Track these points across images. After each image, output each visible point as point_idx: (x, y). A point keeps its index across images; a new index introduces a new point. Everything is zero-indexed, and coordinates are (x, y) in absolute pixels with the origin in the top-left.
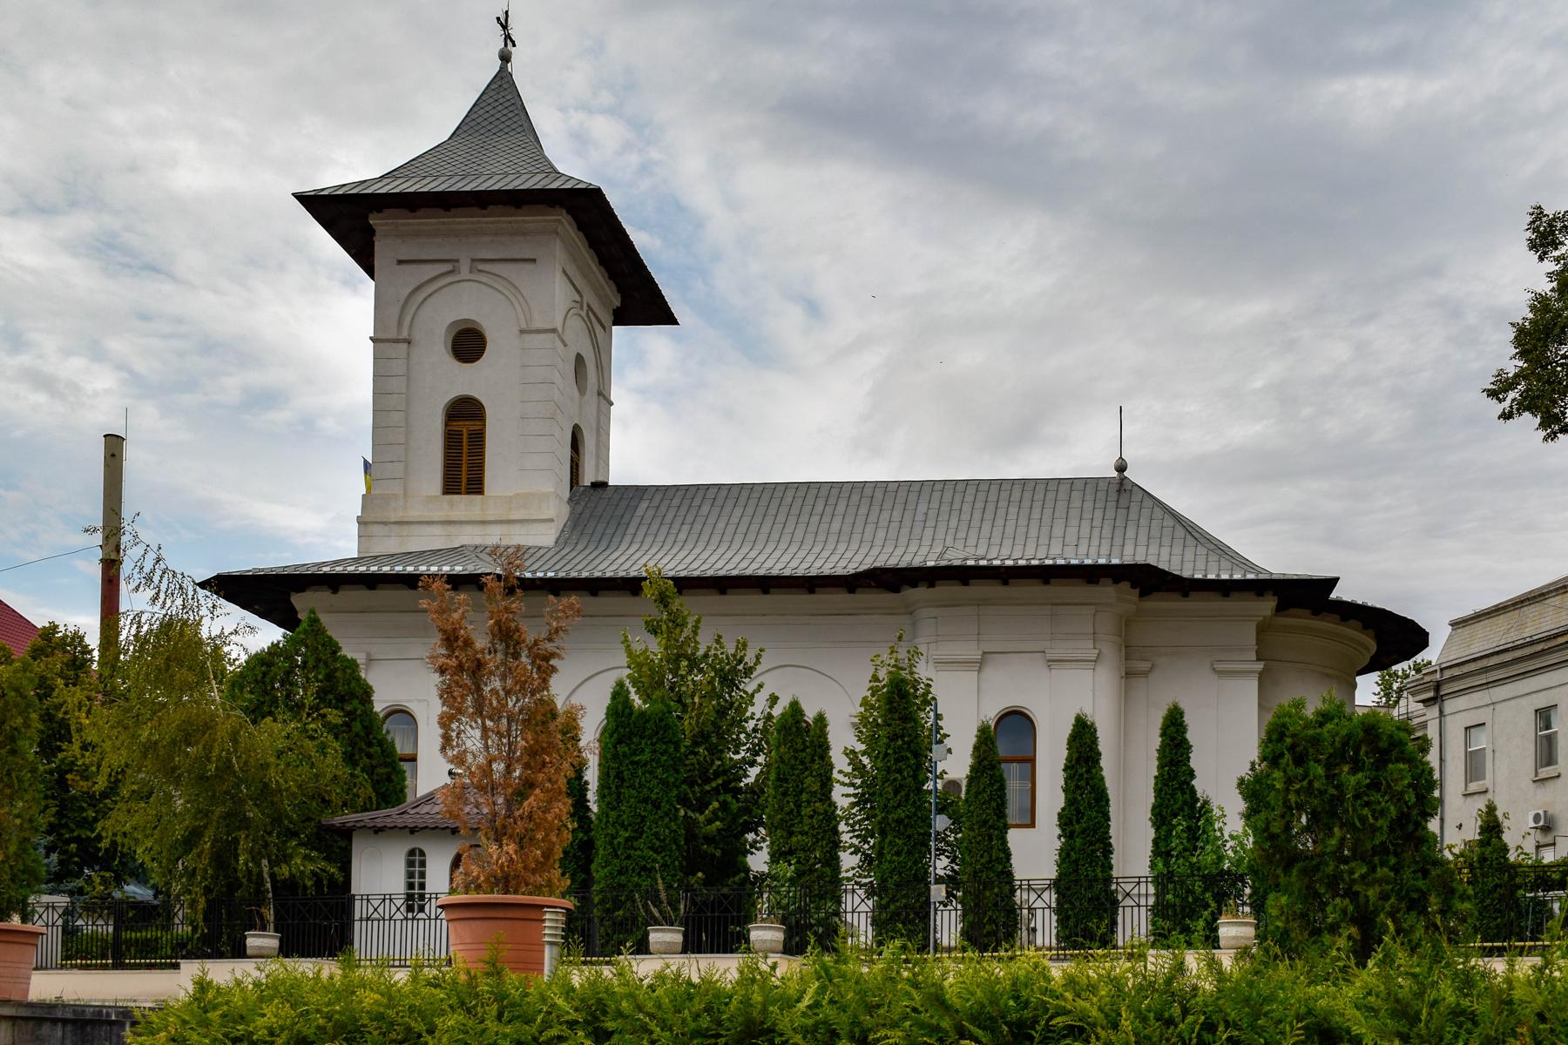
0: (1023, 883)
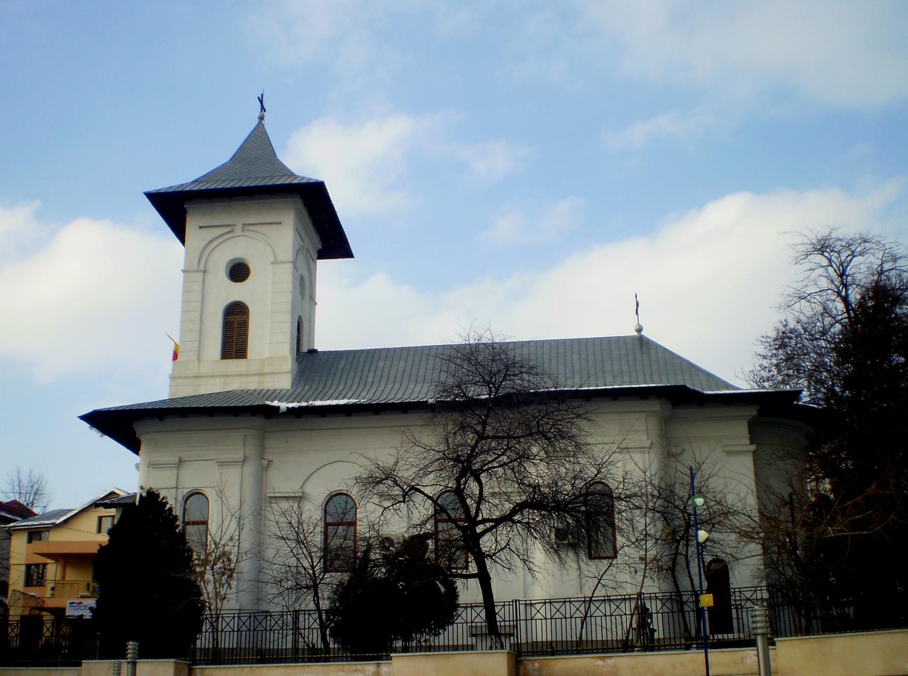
0: (506, 604)
